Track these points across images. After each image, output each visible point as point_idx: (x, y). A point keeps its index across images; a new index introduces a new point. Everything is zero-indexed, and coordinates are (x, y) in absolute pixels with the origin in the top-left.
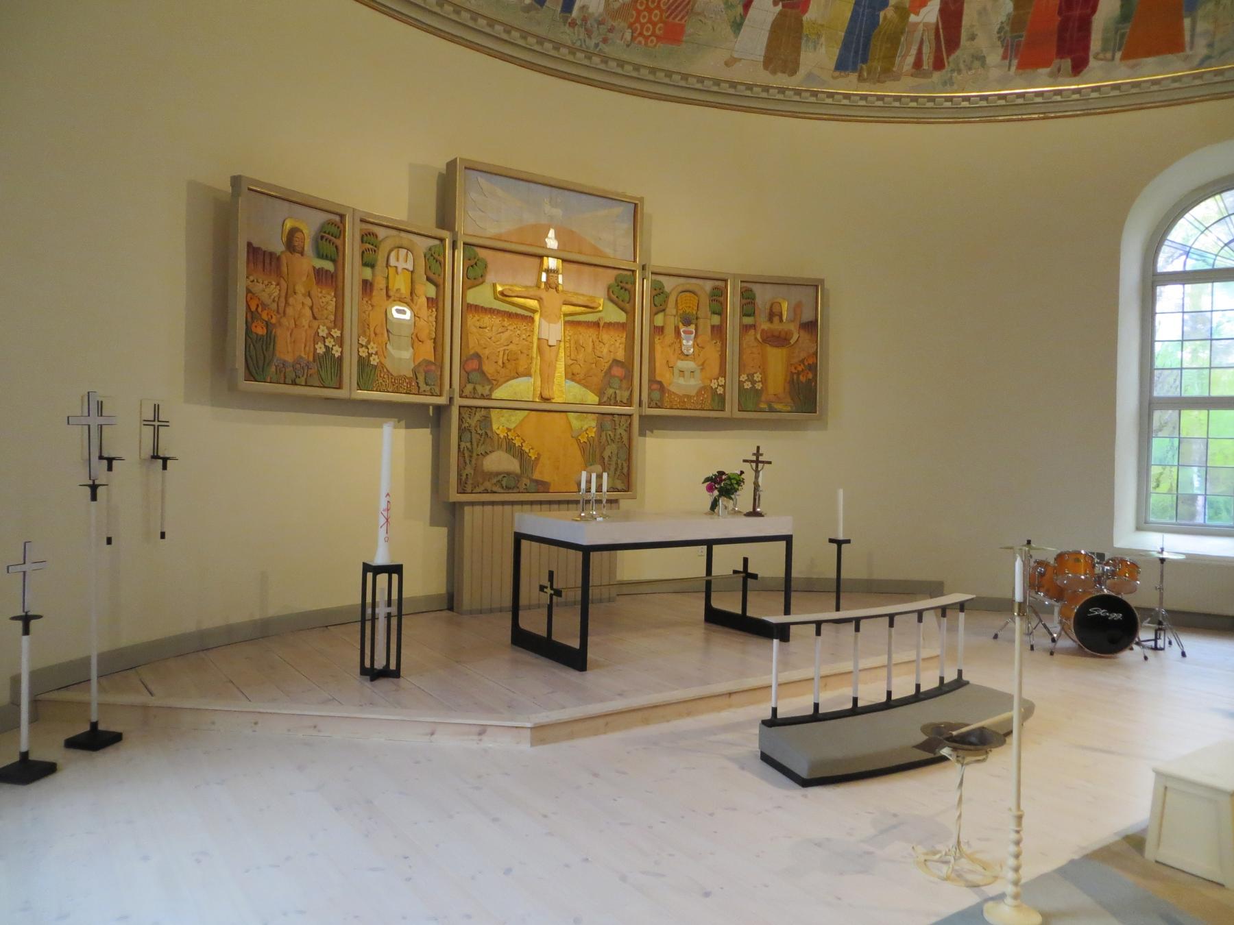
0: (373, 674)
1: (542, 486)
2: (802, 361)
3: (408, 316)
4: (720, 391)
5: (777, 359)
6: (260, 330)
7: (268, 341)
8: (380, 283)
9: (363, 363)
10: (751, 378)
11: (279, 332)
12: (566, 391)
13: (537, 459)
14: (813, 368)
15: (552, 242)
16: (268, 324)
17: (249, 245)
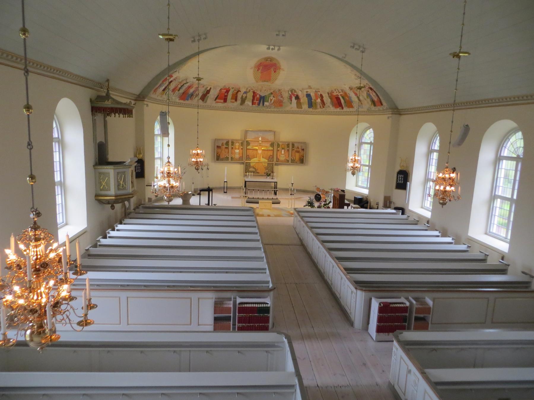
0: (224, 192)
1: (258, 173)
2: (302, 155)
3: (238, 151)
4: (288, 160)
5: (297, 155)
6: (218, 155)
7: (219, 156)
8: (234, 147)
9: (232, 158)
10: (293, 158)
11: (220, 155)
12: (263, 160)
13: (258, 169)
14: (303, 156)
15: (260, 139)
16: (219, 154)
17: (217, 146)
